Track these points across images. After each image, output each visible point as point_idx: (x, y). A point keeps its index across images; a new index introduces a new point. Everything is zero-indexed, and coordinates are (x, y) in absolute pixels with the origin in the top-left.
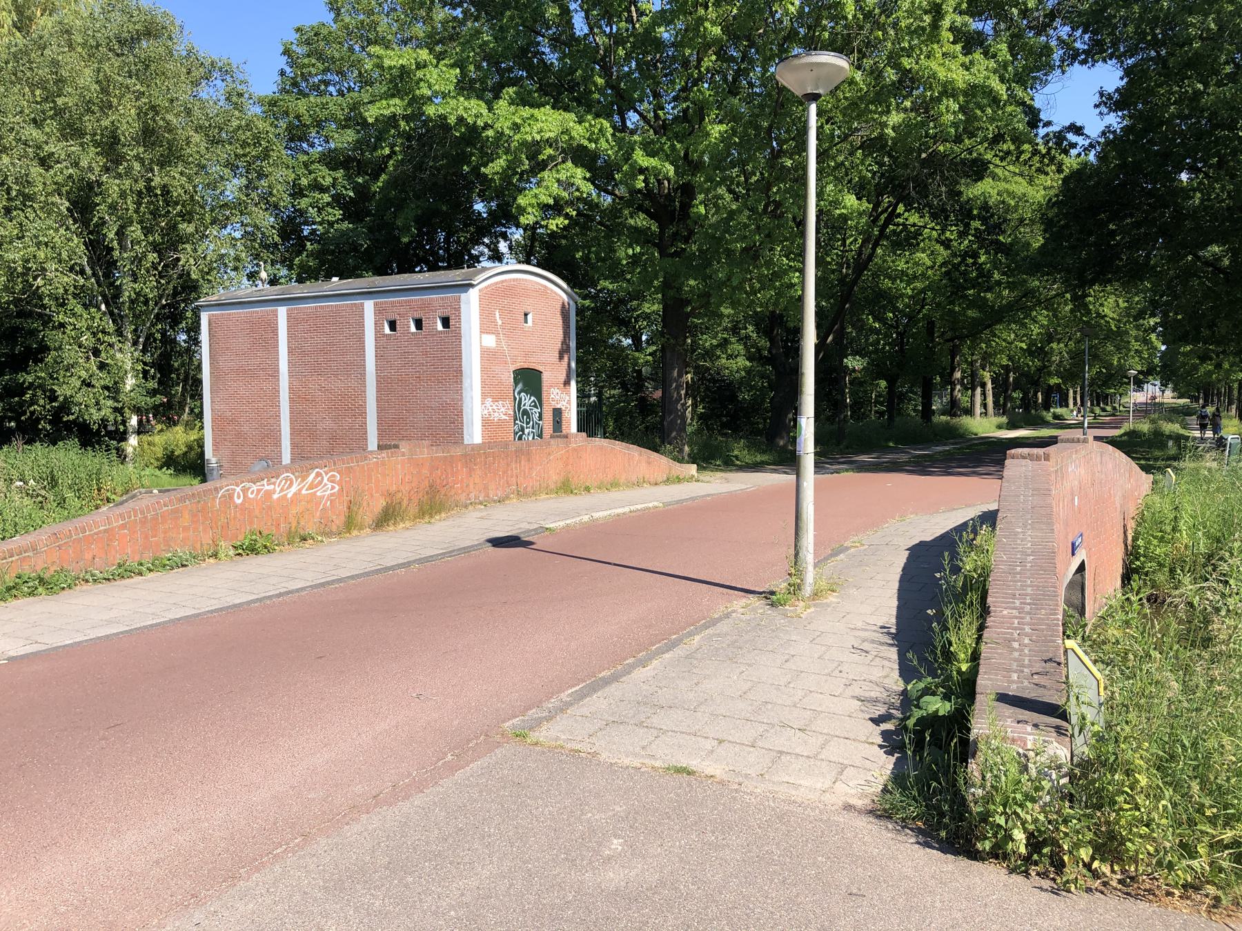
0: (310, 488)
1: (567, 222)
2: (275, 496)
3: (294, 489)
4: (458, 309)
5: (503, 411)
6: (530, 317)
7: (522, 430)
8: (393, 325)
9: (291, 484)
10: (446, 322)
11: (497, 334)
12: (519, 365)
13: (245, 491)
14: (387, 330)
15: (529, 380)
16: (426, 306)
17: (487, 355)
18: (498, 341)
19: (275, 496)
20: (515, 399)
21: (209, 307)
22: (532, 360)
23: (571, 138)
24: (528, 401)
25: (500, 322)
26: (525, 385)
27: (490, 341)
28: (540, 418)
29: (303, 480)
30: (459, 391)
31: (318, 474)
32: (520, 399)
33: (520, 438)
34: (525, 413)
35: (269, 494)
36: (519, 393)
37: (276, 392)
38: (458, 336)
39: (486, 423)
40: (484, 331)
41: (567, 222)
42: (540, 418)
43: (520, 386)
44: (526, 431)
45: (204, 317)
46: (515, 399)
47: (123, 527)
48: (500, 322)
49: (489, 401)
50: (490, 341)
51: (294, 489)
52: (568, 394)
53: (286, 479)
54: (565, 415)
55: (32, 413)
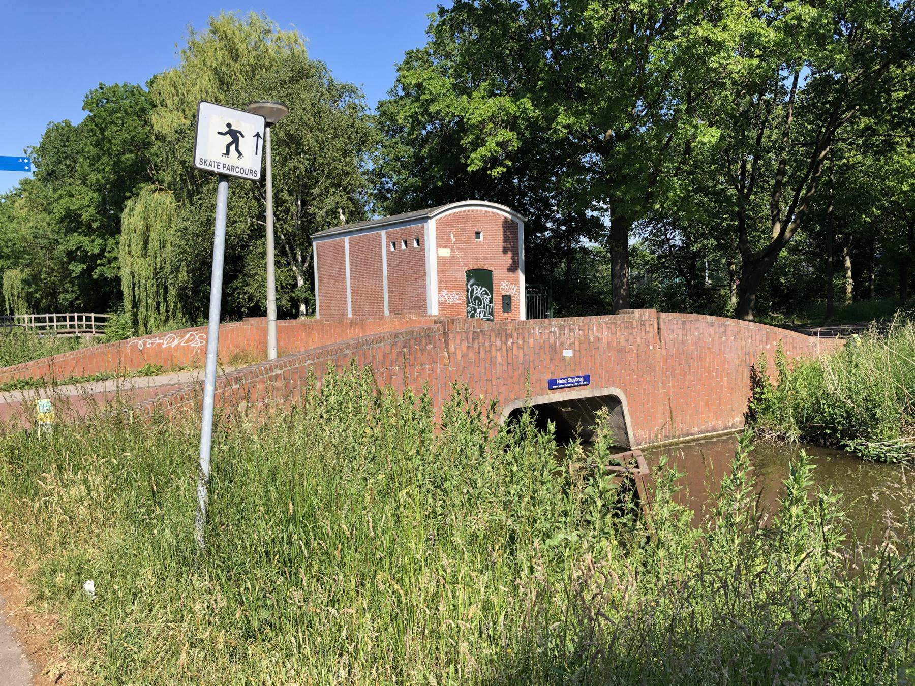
0: (187, 342)
1: (505, 170)
2: (164, 346)
3: (176, 342)
4: (423, 233)
5: (457, 298)
6: (481, 235)
7: (475, 310)
8: (394, 244)
9: (174, 340)
10: (418, 241)
11: (452, 248)
12: (471, 267)
13: (145, 343)
14: (392, 249)
15: (481, 277)
16: (409, 233)
17: (442, 261)
18: (452, 252)
19: (164, 346)
20: (468, 289)
21: (316, 238)
22: (483, 263)
23: (508, 113)
24: (479, 291)
25: (454, 240)
26: (476, 280)
27: (445, 253)
28: (491, 301)
29: (182, 338)
30: (424, 286)
31: (191, 335)
32: (473, 290)
33: (473, 316)
34: (477, 298)
35: (160, 345)
36: (471, 286)
37: (345, 288)
38: (423, 251)
39: (442, 306)
40: (440, 245)
41: (505, 170)
42: (491, 301)
43: (472, 281)
44: (478, 311)
45: (315, 244)
46: (468, 289)
47: (73, 359)
48: (454, 240)
49: (444, 292)
50: (445, 253)
51: (176, 342)
52: (517, 283)
53: (171, 337)
54: (514, 300)
55: (239, 303)
